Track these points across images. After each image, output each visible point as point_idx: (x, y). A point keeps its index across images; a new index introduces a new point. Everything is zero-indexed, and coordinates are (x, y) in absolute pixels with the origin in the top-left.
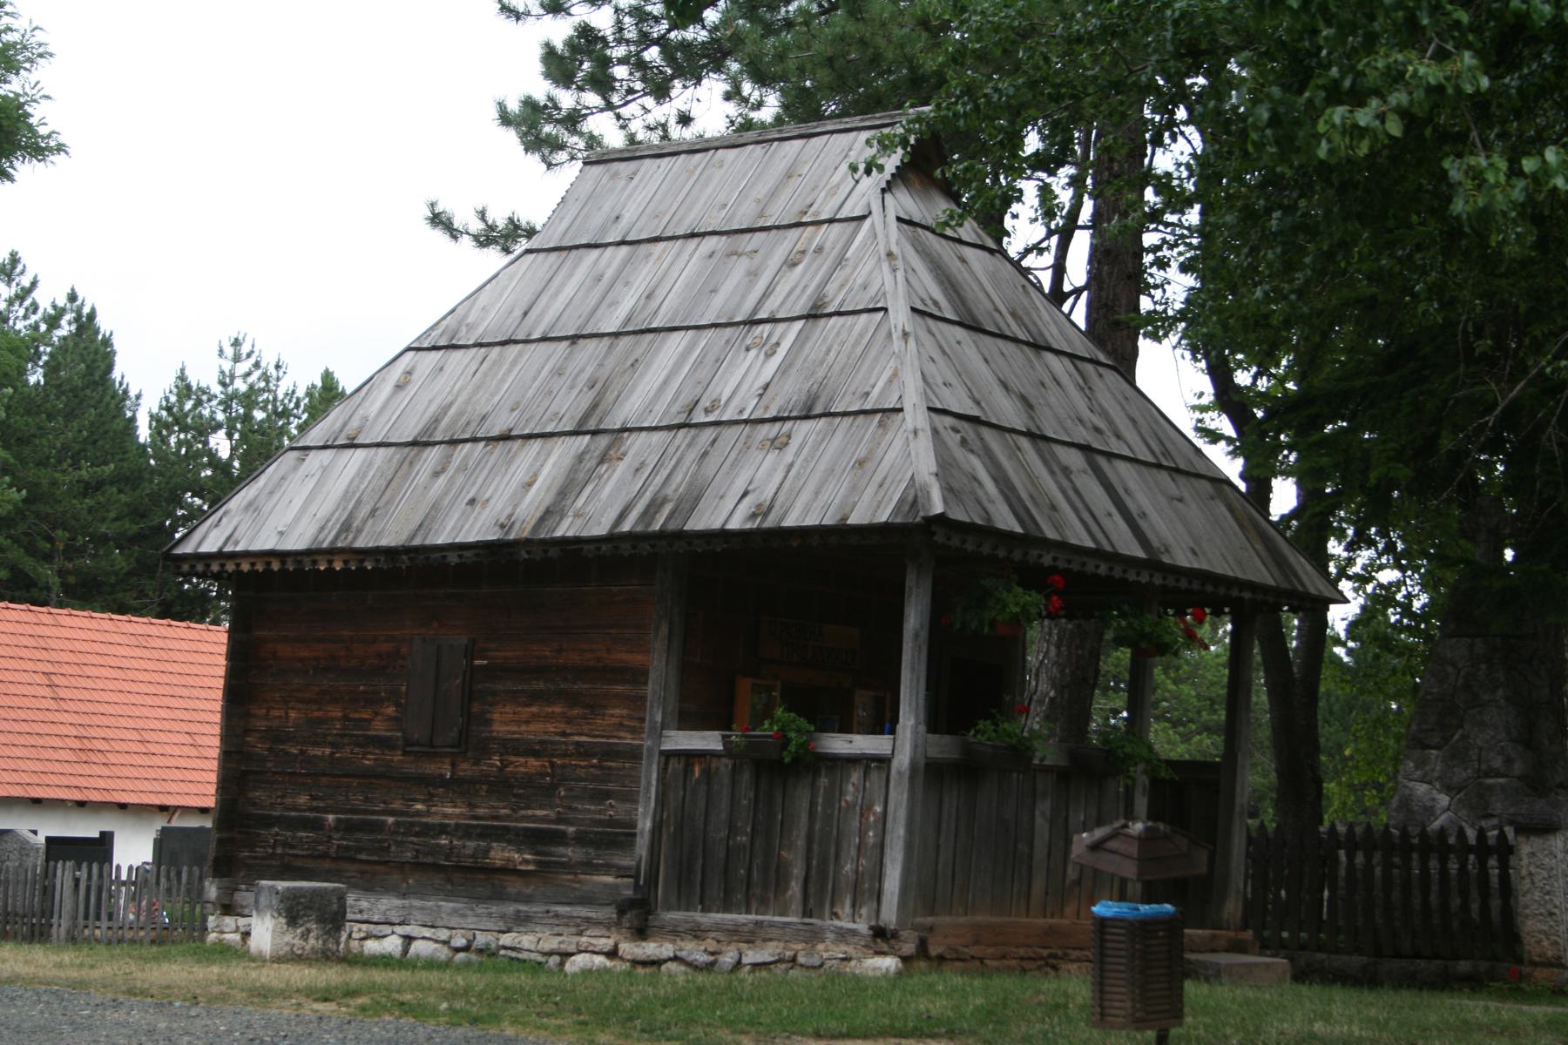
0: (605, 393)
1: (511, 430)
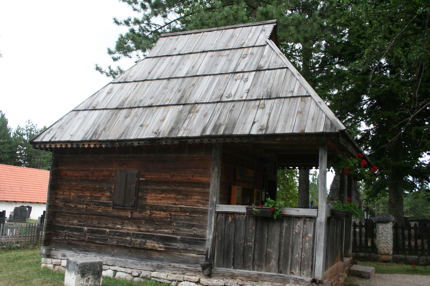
0: (185, 93)
1: (152, 104)
